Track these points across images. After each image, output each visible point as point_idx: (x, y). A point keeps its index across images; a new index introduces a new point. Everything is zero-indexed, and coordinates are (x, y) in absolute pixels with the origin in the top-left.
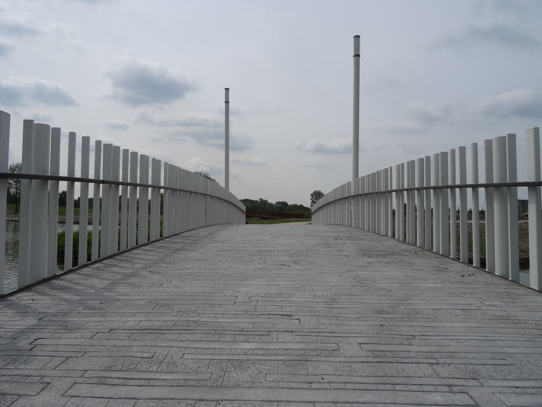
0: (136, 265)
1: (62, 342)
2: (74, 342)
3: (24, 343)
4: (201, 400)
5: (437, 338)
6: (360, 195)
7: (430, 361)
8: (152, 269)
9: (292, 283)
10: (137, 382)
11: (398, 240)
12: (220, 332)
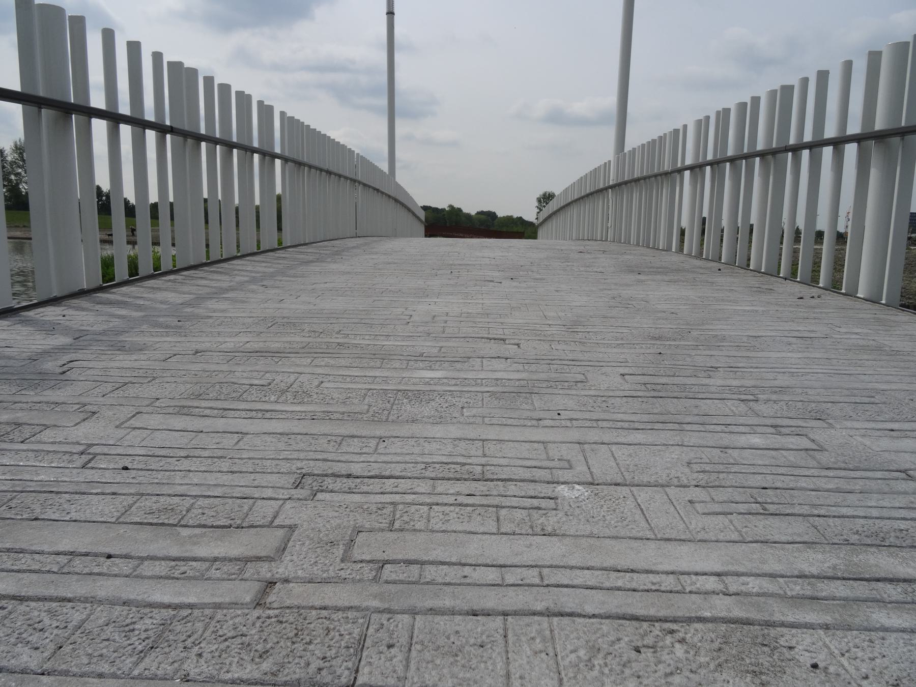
0: (238, 279)
1: (113, 364)
2: (136, 364)
3: (50, 365)
4: (353, 437)
5: (756, 370)
6: (626, 183)
7: (743, 397)
8: (265, 283)
9: (507, 301)
10: (243, 414)
11: (689, 255)
12: (383, 357)
